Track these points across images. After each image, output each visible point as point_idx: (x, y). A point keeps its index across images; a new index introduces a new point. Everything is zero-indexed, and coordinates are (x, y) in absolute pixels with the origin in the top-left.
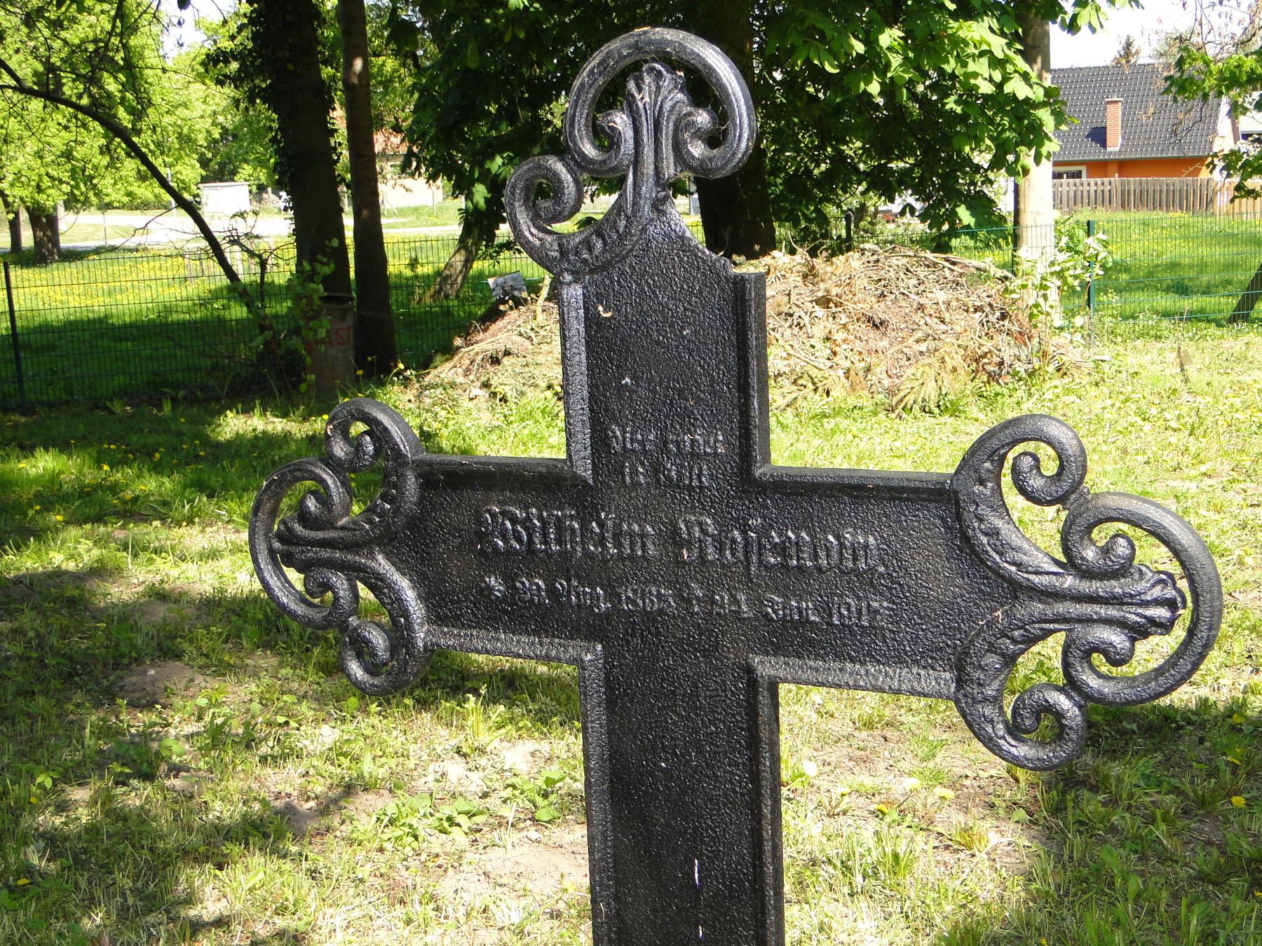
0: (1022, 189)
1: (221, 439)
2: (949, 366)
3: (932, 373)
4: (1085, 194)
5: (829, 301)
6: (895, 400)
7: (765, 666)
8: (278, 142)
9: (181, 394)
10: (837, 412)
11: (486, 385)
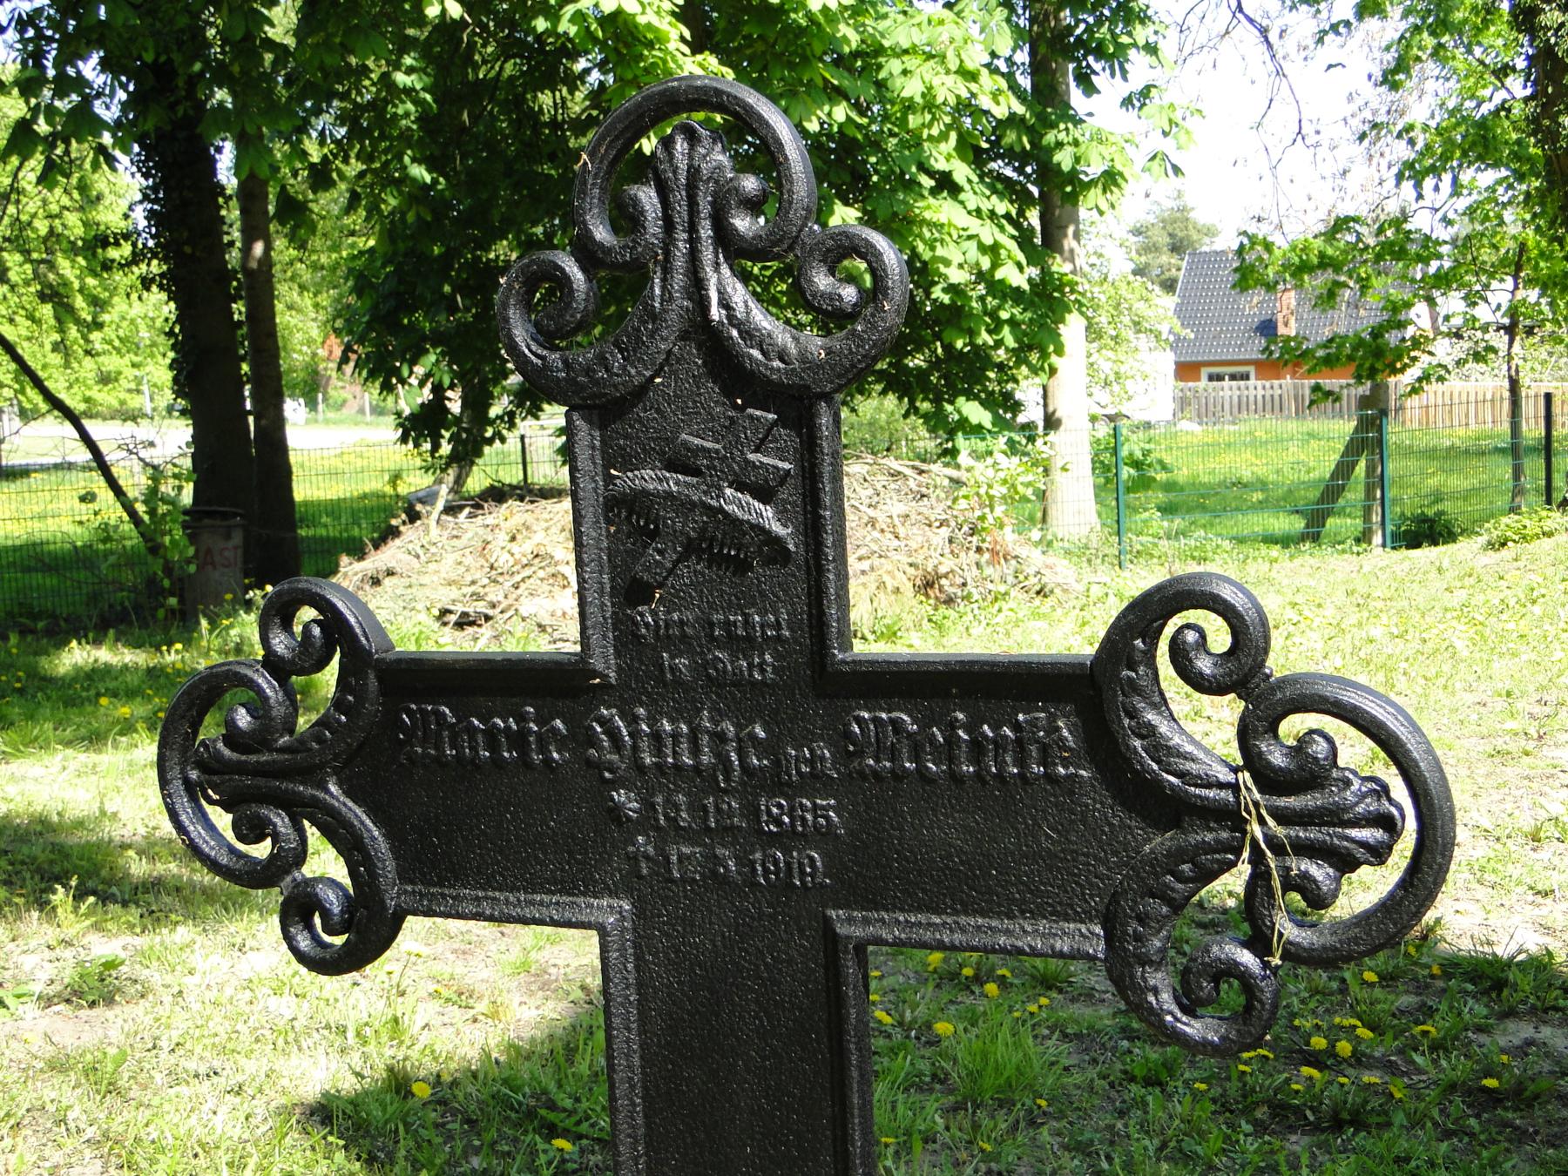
0: (1050, 390)
2: (889, 588)
4: (1252, 399)
7: (848, 925)
8: (176, 336)
9: (41, 625)
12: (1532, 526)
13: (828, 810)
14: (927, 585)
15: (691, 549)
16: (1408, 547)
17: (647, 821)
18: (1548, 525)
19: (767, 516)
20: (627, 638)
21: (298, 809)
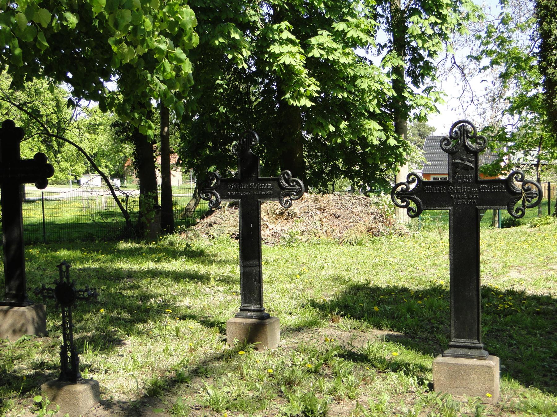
1: (120, 249)
2: (360, 230)
3: (354, 232)
5: (321, 209)
6: (341, 240)
10: (322, 243)
11: (207, 233)
12: (544, 221)
13: (477, 196)
14: (370, 230)
15: (462, 168)
16: (506, 227)
17: (455, 198)
18: (549, 221)
19: (471, 165)
20: (454, 178)
21: (409, 198)
